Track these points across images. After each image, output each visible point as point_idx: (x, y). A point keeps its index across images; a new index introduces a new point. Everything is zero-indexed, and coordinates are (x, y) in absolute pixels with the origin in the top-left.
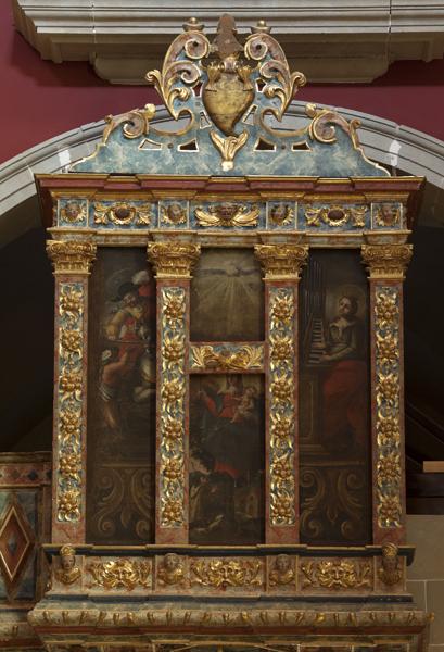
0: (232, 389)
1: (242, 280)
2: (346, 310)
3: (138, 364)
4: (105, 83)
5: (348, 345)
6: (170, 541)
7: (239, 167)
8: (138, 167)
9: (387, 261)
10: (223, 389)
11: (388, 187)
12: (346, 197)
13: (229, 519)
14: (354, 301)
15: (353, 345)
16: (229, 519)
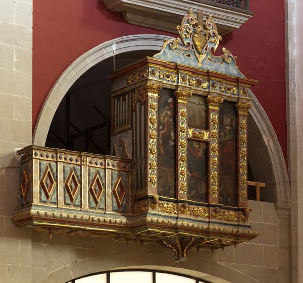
0: (197, 146)
1: (200, 107)
2: (230, 123)
3: (170, 133)
4: (126, 22)
5: (230, 136)
6: (182, 198)
7: (203, 66)
8: (174, 60)
9: (154, 89)
10: (195, 146)
11: (248, 83)
12: (233, 83)
13: (200, 195)
14: (232, 120)
15: (232, 136)
16: (200, 195)
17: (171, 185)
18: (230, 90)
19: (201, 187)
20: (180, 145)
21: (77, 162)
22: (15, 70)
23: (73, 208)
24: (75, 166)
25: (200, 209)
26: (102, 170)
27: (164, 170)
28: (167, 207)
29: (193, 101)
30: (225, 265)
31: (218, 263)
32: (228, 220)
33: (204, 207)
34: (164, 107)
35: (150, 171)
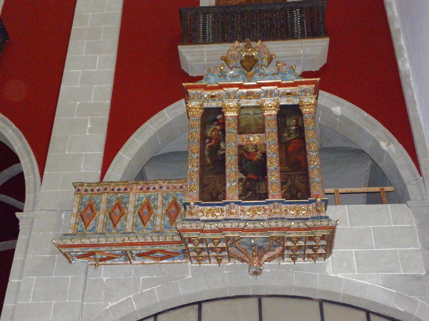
2: (295, 124)
22: (88, 134)
30: (341, 277)
31: (332, 275)
34: (211, 124)
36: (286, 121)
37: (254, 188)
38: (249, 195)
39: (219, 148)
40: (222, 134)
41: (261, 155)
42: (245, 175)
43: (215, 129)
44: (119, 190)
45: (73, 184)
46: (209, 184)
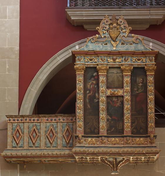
0: (116, 99)
1: (118, 74)
2: (141, 81)
6: (103, 134)
7: (117, 49)
13: (116, 129)
17: (96, 127)
18: (92, 60)
19: (119, 125)
20: (101, 101)
21: (18, 121)
22: (7, 73)
23: (19, 148)
24: (36, 124)
25: (142, 139)
26: (58, 123)
27: (91, 118)
28: (139, 141)
29: (112, 72)
30: (162, 172)
31: (157, 171)
32: (139, 144)
33: (119, 138)
34: (90, 79)
35: (78, 120)
36: (136, 79)
37: (116, 129)
38: (113, 130)
39: (94, 97)
40: (97, 87)
41: (120, 103)
42: (111, 117)
43: (92, 83)
44: (34, 120)
45: (6, 116)
46: (89, 122)
